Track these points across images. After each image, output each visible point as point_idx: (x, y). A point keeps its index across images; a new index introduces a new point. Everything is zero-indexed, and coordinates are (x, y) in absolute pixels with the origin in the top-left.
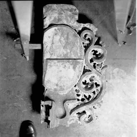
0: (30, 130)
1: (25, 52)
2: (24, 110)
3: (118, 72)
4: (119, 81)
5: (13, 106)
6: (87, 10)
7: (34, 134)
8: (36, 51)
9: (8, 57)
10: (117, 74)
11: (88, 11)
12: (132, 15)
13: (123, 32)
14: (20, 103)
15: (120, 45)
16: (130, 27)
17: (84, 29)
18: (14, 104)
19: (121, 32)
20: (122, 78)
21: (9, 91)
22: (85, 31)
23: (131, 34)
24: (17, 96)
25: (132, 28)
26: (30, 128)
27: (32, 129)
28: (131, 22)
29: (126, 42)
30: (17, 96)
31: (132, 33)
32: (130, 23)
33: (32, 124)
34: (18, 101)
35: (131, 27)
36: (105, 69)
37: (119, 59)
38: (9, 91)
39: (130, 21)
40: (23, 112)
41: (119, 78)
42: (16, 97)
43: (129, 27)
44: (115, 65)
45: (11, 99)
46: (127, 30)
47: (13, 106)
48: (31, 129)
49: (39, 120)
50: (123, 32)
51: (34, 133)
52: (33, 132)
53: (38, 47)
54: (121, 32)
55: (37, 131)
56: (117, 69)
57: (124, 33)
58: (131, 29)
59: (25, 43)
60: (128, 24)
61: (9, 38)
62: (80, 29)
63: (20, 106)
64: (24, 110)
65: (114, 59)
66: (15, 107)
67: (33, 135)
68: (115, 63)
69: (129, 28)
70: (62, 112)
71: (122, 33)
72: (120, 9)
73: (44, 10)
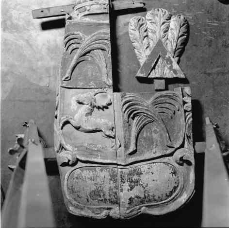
1: (213, 131)
31: (8, 151)
32: (19, 156)
43: (22, 149)
44: (45, 91)
46: (24, 144)
50: (30, 142)
66: (217, 20)
71: (33, 140)
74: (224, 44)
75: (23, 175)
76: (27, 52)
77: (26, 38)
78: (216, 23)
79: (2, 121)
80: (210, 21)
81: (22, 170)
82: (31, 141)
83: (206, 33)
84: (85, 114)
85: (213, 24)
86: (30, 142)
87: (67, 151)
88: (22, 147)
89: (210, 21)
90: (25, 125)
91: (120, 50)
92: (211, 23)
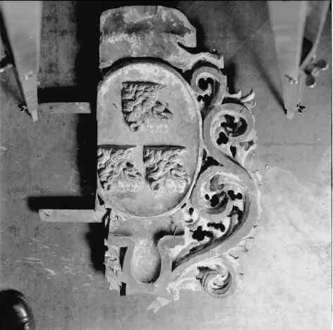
0: (16, 316)
3: (277, 177)
4: (279, 198)
5: (25, 264)
7: (27, 324)
8: (82, 116)
10: (274, 181)
12: (314, 36)
13: (294, 81)
14: (40, 256)
15: (290, 115)
16: (311, 70)
17: (201, 64)
18: (29, 260)
20: (289, 189)
21: (13, 229)
22: (201, 69)
26: (17, 310)
27: (24, 314)
28: (315, 56)
29: (304, 107)
31: (315, 84)
32: (312, 59)
33: (21, 300)
34: (37, 252)
35: (315, 70)
37: (279, 144)
38: (13, 229)
39: (313, 55)
40: (49, 278)
41: (281, 192)
42: (31, 241)
43: (310, 68)
45: (18, 246)
46: (304, 76)
47: (25, 264)
48: (19, 313)
50: (296, 79)
51: (27, 322)
52: (26, 319)
53: (84, 108)
55: (35, 314)
57: (297, 82)
58: (313, 73)
59: (27, 78)
60: (306, 62)
62: (190, 67)
67: (27, 328)
68: (269, 155)
69: (308, 72)
71: (292, 82)
72: (286, 25)
73: (104, 18)
76: (296, 214)
77: (298, 234)
92: (36, 261)
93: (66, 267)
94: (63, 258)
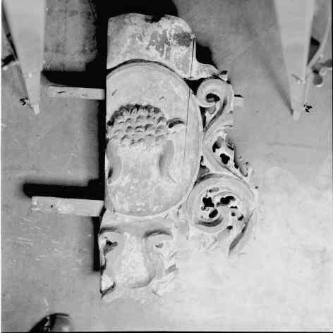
2: (40, 256)
6: (213, 21)
9: (11, 121)
11: (214, 23)
19: (298, 79)
23: (319, 86)
24: (25, 219)
25: (323, 72)
30: (25, 219)
31: (323, 84)
35: (322, 69)
36: (71, 92)
37: (283, 145)
43: (317, 67)
46: (312, 76)
49: (80, 300)
50: (303, 79)
54: (298, 79)
56: (276, 169)
59: (30, 75)
61: (154, 23)
63: (32, 244)
64: (40, 256)
65: (271, 144)
66: (19, 245)
70: (142, 273)
71: (299, 82)
74: (10, 210)
75: (313, 30)
78: (20, 240)
79: (6, 316)
80: (28, 243)
81: (316, 38)
82: (302, 81)
83: (36, 227)
84: (163, 248)
85: (24, 239)
86: (303, 79)
87: (192, 185)
88: (316, 72)
89: (28, 243)
90: (310, 107)
91: (73, 182)
93: (56, 250)
94: (54, 242)
